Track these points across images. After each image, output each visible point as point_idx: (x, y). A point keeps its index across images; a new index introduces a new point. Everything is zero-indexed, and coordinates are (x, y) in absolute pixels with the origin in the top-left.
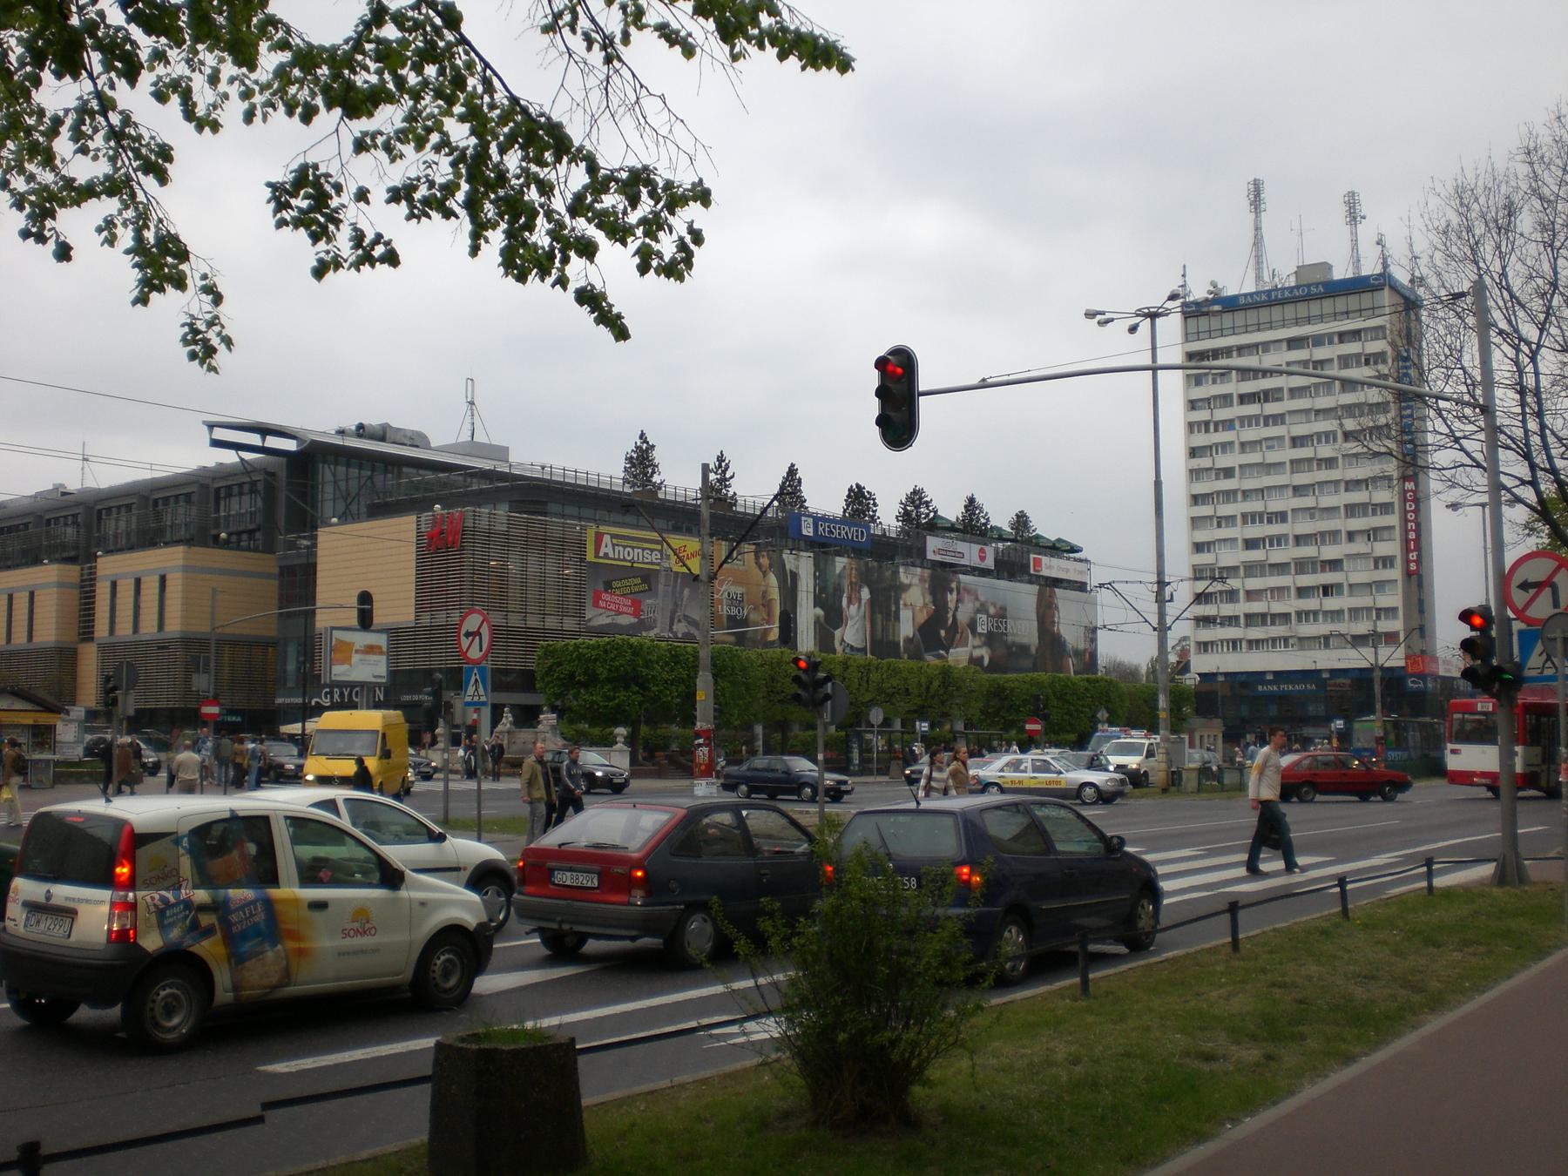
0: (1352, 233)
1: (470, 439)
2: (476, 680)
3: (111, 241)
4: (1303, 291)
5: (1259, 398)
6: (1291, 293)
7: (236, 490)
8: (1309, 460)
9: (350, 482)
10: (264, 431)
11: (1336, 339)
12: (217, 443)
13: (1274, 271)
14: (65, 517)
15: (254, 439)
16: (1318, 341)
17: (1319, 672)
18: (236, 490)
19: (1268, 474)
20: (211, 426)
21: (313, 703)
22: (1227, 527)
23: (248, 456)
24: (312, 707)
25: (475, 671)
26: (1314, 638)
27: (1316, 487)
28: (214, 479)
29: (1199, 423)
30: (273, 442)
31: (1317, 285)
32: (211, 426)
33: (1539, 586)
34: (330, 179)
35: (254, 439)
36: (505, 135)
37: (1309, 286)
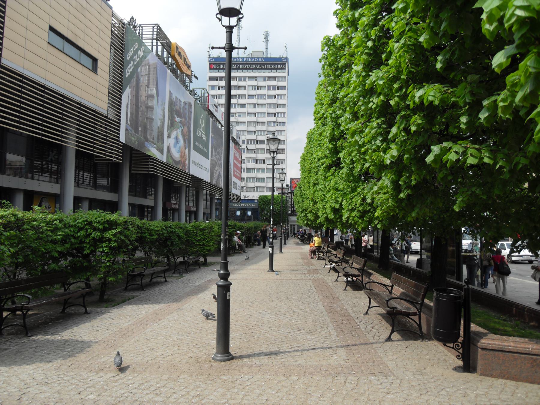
3: (320, 62)
4: (256, 60)
6: (252, 60)
8: (254, 122)
11: (267, 79)
17: (254, 200)
22: (222, 90)
26: (253, 113)
27: (257, 114)
31: (262, 58)
37: (258, 58)
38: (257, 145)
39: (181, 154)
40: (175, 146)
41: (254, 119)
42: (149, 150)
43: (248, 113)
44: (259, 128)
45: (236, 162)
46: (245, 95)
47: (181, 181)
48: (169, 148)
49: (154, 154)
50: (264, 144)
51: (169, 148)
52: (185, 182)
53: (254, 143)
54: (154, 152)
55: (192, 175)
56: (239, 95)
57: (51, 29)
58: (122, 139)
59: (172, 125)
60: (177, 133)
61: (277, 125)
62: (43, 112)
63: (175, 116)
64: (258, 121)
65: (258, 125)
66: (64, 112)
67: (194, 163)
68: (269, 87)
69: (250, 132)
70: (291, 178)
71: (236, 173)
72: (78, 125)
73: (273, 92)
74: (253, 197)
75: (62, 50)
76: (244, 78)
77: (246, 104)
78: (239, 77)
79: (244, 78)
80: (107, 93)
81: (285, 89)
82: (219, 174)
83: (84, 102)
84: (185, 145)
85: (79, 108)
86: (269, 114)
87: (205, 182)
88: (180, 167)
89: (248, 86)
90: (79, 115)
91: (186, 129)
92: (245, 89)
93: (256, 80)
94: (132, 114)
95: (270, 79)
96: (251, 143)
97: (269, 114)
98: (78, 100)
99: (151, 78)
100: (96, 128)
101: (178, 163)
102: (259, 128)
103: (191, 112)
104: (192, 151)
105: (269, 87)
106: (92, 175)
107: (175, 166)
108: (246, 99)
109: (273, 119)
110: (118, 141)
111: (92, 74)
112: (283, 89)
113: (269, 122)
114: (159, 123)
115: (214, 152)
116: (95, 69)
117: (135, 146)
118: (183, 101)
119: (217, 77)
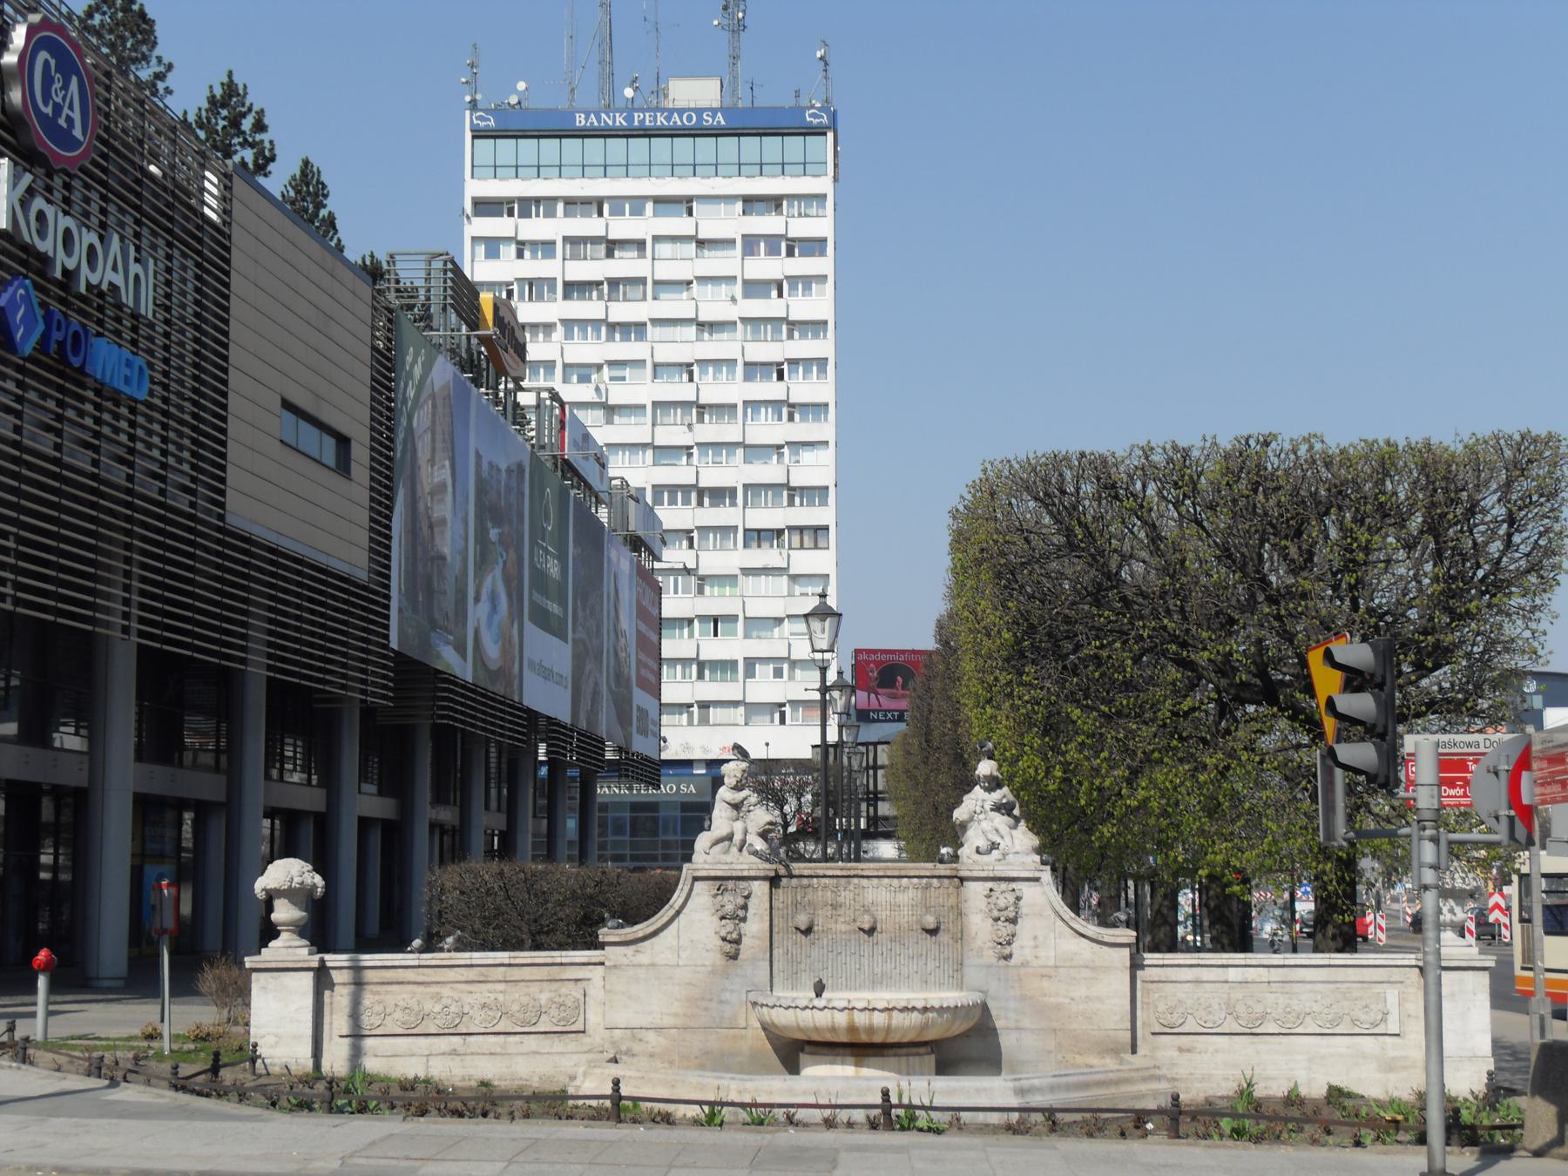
4: (690, 119)
6: (668, 119)
16: (526, 206)
17: (688, 763)
27: (695, 368)
37: (699, 111)
38: (699, 511)
39: (503, 645)
40: (490, 625)
41: (684, 392)
42: (439, 656)
43: (656, 366)
44: (710, 431)
45: (643, 627)
46: (643, 281)
47: (343, 687)
48: (477, 632)
49: (448, 665)
50: (734, 504)
51: (477, 632)
52: (483, 729)
53: (686, 502)
54: (450, 660)
55: (529, 711)
56: (614, 283)
57: (287, 405)
58: (394, 645)
59: (483, 562)
60: (494, 579)
61: (791, 418)
62: (19, 513)
63: (490, 525)
64: (702, 401)
65: (701, 420)
66: (168, 541)
67: (531, 662)
68: (750, 244)
69: (664, 453)
70: (858, 652)
71: (643, 672)
72: (271, 609)
73: (765, 267)
74: (687, 747)
75: (293, 444)
76: (637, 204)
77: (645, 324)
78: (610, 198)
79: (637, 204)
80: (366, 523)
81: (823, 253)
82: (595, 689)
83: (286, 544)
84: (511, 614)
85: (272, 563)
86: (753, 369)
87: (456, 684)
88: (499, 688)
89: (656, 239)
90: (162, 525)
91: (513, 555)
92: (642, 255)
93: (690, 214)
94: (407, 558)
95: (758, 206)
96: (673, 502)
97: (753, 369)
98: (272, 538)
99: (439, 437)
100: (218, 567)
101: (494, 675)
102: (710, 431)
103: (523, 494)
104: (528, 624)
105: (750, 244)
106: (299, 743)
107: (490, 688)
108: (644, 298)
109: (771, 389)
110: (386, 647)
111: (335, 480)
112: (812, 255)
113: (753, 405)
114: (458, 565)
115: (579, 610)
116: (343, 466)
117: (414, 654)
118: (503, 467)
119: (511, 201)
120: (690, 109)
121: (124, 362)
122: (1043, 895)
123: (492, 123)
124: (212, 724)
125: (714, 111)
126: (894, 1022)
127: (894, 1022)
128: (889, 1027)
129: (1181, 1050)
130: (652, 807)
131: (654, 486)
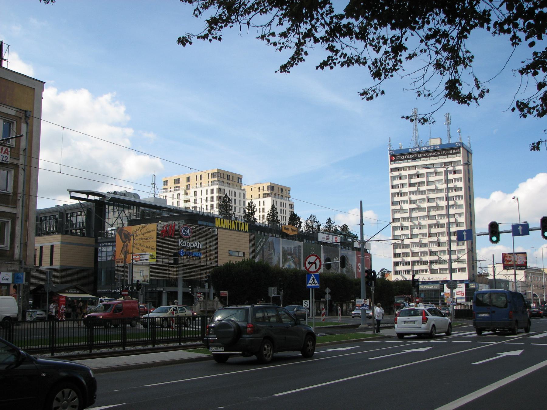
0: (447, 128)
1: (154, 196)
2: (313, 279)
4: (432, 147)
5: (399, 186)
6: (428, 148)
7: (48, 218)
9: (134, 210)
10: (88, 193)
12: (72, 198)
13: (421, 141)
14: (50, 216)
15: (84, 196)
16: (402, 169)
18: (48, 218)
19: (420, 212)
20: (70, 192)
21: (113, 291)
23: (81, 202)
24: (113, 293)
25: (313, 275)
28: (65, 211)
29: (395, 193)
30: (91, 197)
32: (70, 192)
33: (312, 263)
34: (335, 18)
35: (84, 196)
36: (357, 19)
37: (434, 146)
119: (398, 168)
120: (432, 146)
121: (512, 108)
122: (219, 302)
123: (393, 153)
124: (458, 301)
125: (437, 145)
126: (124, 306)
127: (124, 306)
128: (122, 307)
129: (488, 309)
130: (283, 300)
131: (428, 224)
